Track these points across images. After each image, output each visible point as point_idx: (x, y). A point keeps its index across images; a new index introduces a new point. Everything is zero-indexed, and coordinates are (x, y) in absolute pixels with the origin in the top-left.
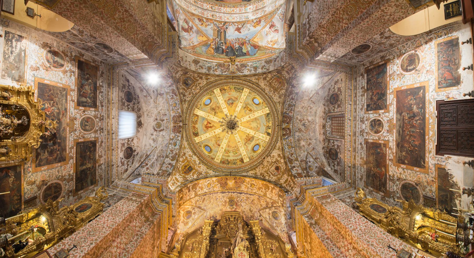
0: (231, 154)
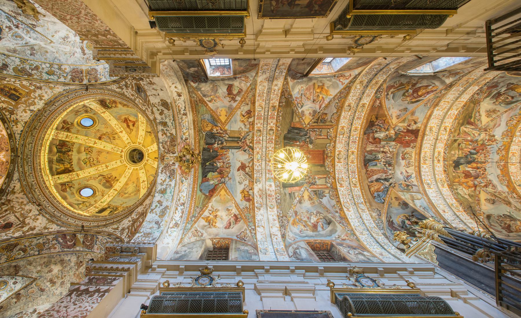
0: (83, 156)
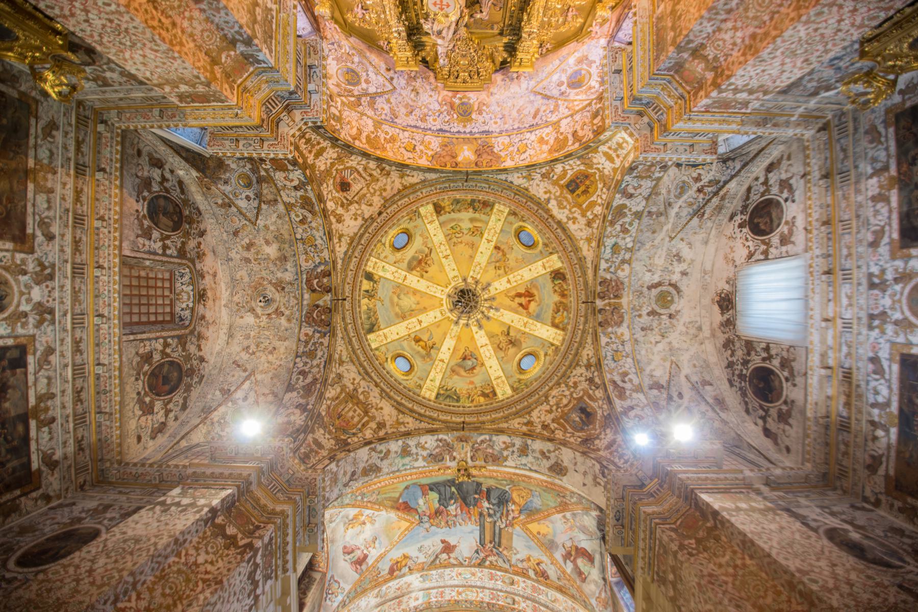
0: (466, 225)
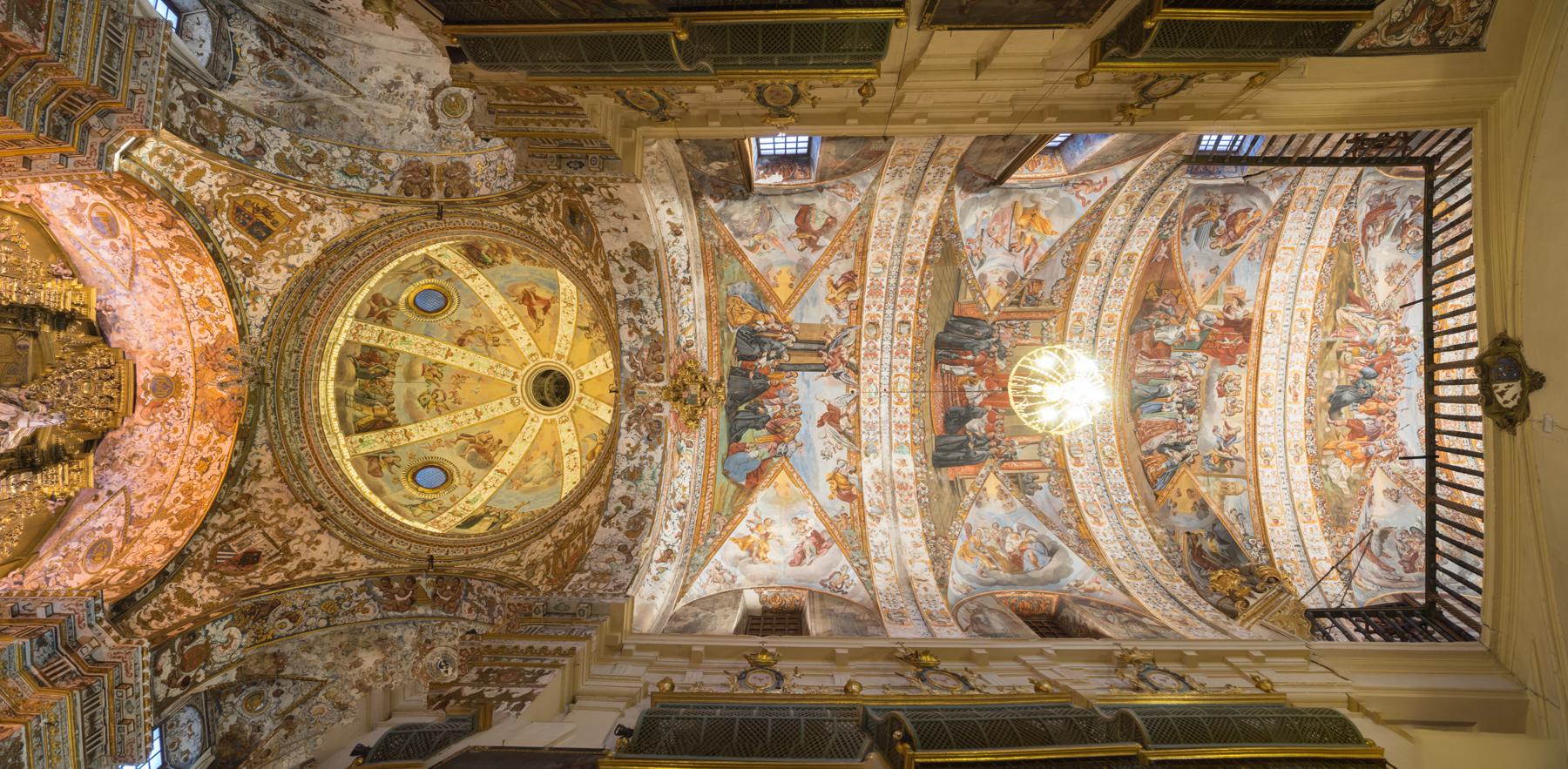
0: (420, 387)
